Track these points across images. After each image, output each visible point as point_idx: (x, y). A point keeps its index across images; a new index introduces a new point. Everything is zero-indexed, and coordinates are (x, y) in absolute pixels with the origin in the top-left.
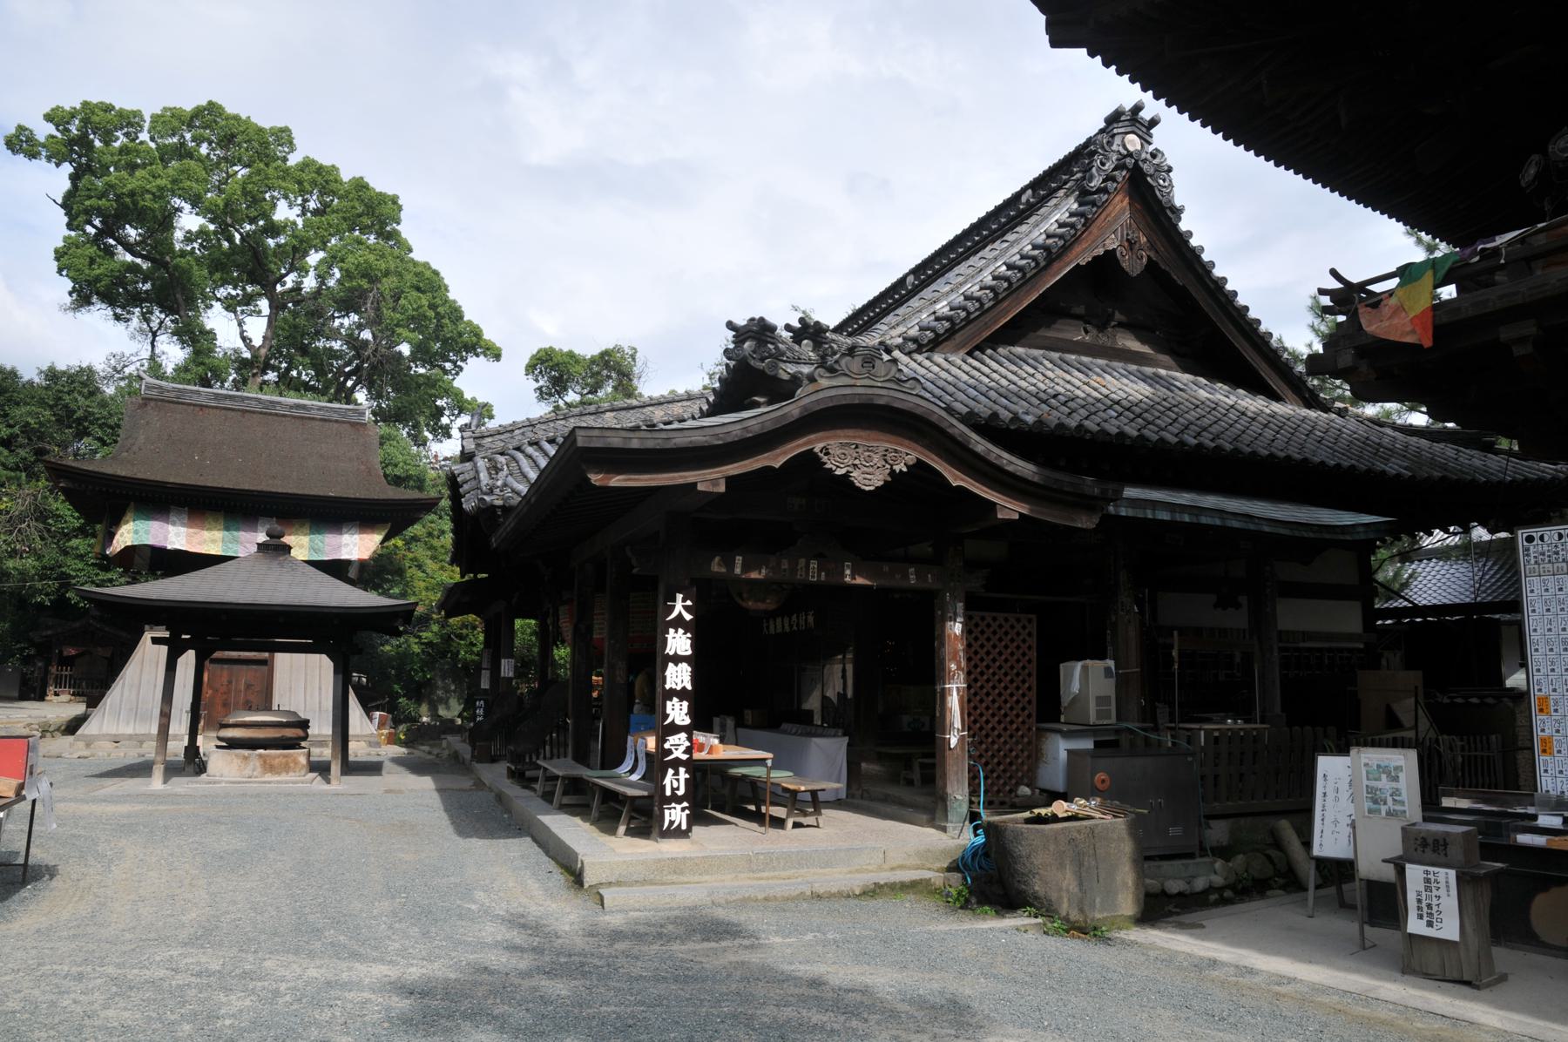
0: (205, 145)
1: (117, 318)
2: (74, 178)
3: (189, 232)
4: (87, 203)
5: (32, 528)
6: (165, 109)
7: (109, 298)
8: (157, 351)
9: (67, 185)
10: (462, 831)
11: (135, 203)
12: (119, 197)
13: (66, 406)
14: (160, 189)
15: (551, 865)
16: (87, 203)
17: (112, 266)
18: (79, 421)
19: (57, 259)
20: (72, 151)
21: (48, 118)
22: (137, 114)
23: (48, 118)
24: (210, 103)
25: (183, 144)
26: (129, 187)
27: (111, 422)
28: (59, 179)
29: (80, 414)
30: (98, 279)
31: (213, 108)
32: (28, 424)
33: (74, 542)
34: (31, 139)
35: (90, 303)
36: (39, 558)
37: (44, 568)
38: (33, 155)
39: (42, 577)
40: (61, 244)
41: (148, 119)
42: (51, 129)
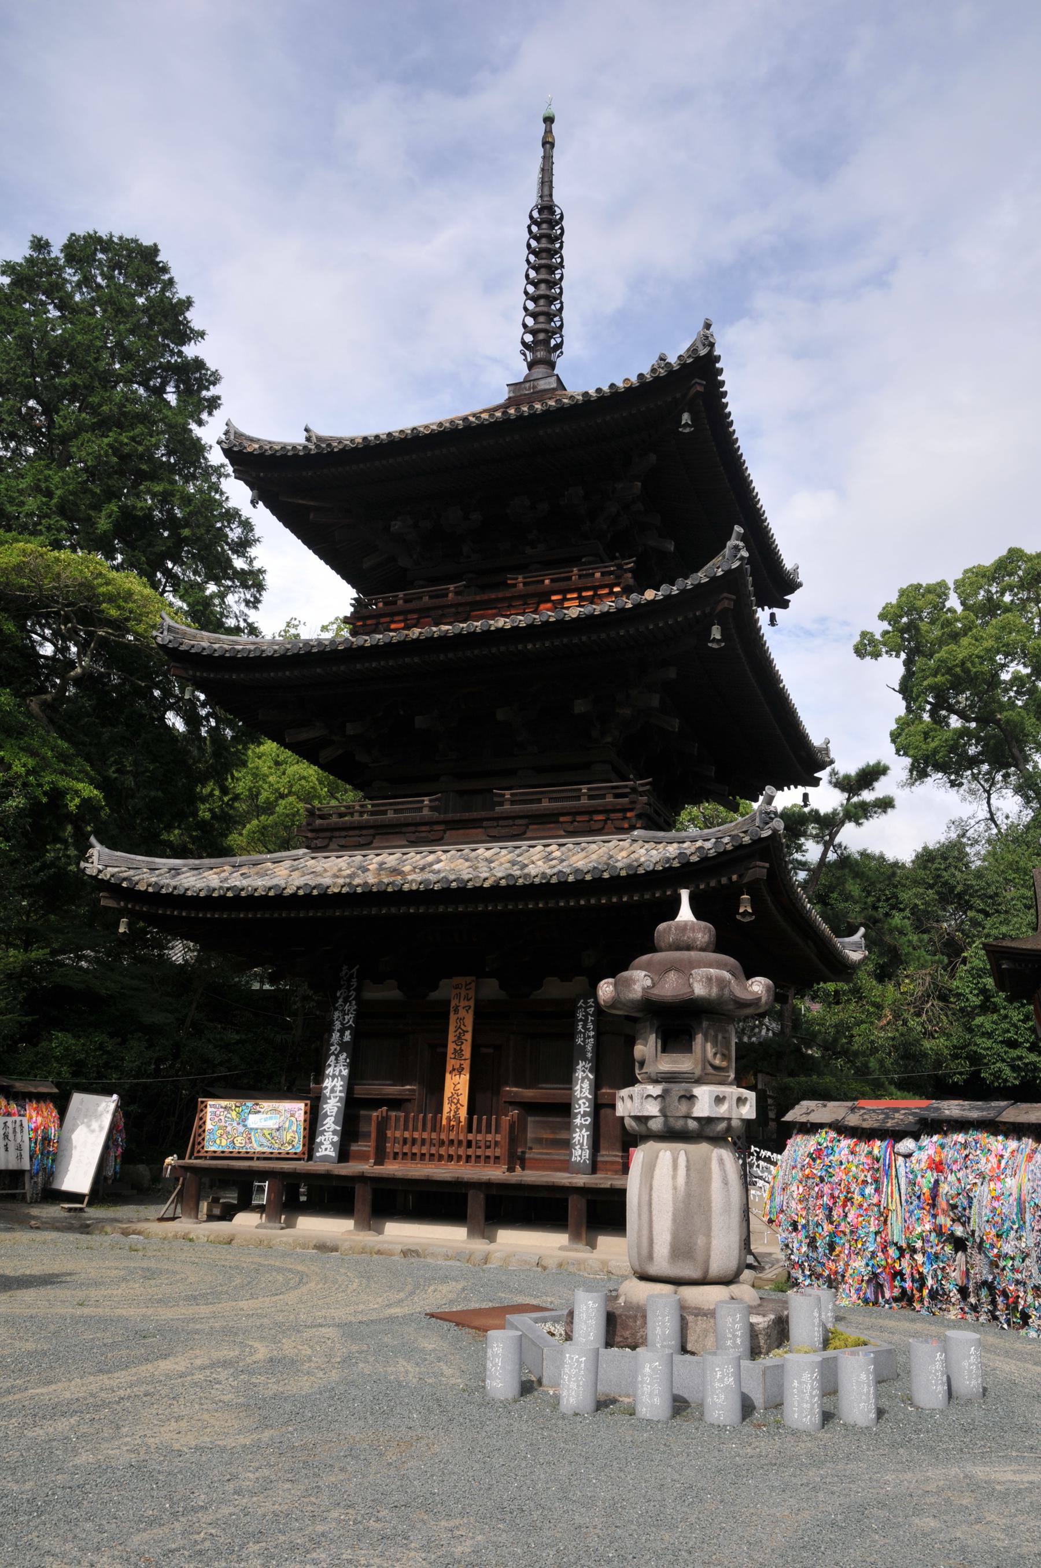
0: (1007, 594)
1: (953, 784)
2: (908, 663)
3: (298, 635)
4: (925, 683)
5: (933, 1004)
6: (966, 572)
7: (942, 767)
8: (993, 809)
9: (901, 671)
10: (231, 1220)
11: (967, 671)
12: (949, 671)
13: (946, 883)
14: (988, 650)
15: (678, 1335)
16: (925, 683)
17: (947, 735)
18: (960, 896)
19: (893, 741)
20: (903, 639)
21: (882, 617)
22: (942, 584)
23: (882, 617)
24: (1010, 550)
25: (989, 599)
26: (960, 657)
27: (990, 891)
28: (892, 668)
29: (959, 888)
30: (935, 751)
31: (1015, 555)
32: (916, 905)
33: (979, 1020)
34: (872, 641)
35: (926, 775)
36: (948, 1036)
37: (955, 1047)
38: (876, 655)
39: (955, 1057)
40: (895, 726)
41: (952, 586)
42: (885, 626)
